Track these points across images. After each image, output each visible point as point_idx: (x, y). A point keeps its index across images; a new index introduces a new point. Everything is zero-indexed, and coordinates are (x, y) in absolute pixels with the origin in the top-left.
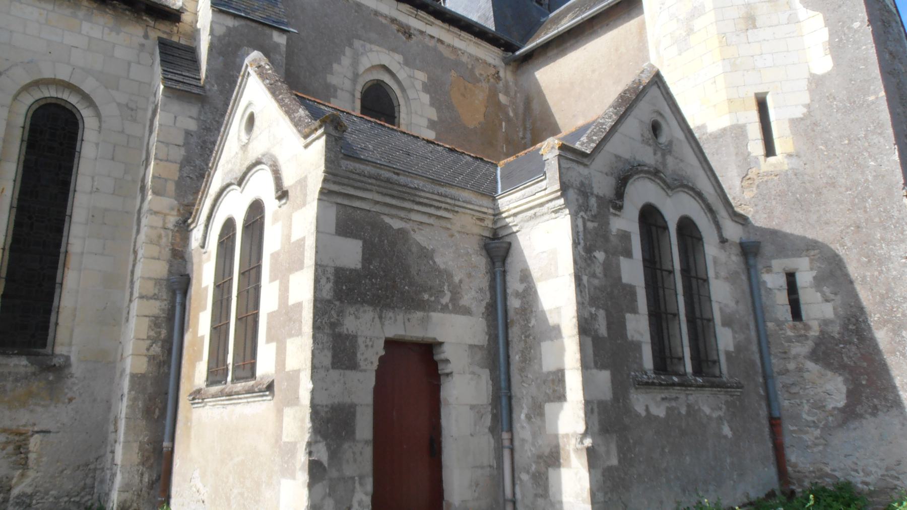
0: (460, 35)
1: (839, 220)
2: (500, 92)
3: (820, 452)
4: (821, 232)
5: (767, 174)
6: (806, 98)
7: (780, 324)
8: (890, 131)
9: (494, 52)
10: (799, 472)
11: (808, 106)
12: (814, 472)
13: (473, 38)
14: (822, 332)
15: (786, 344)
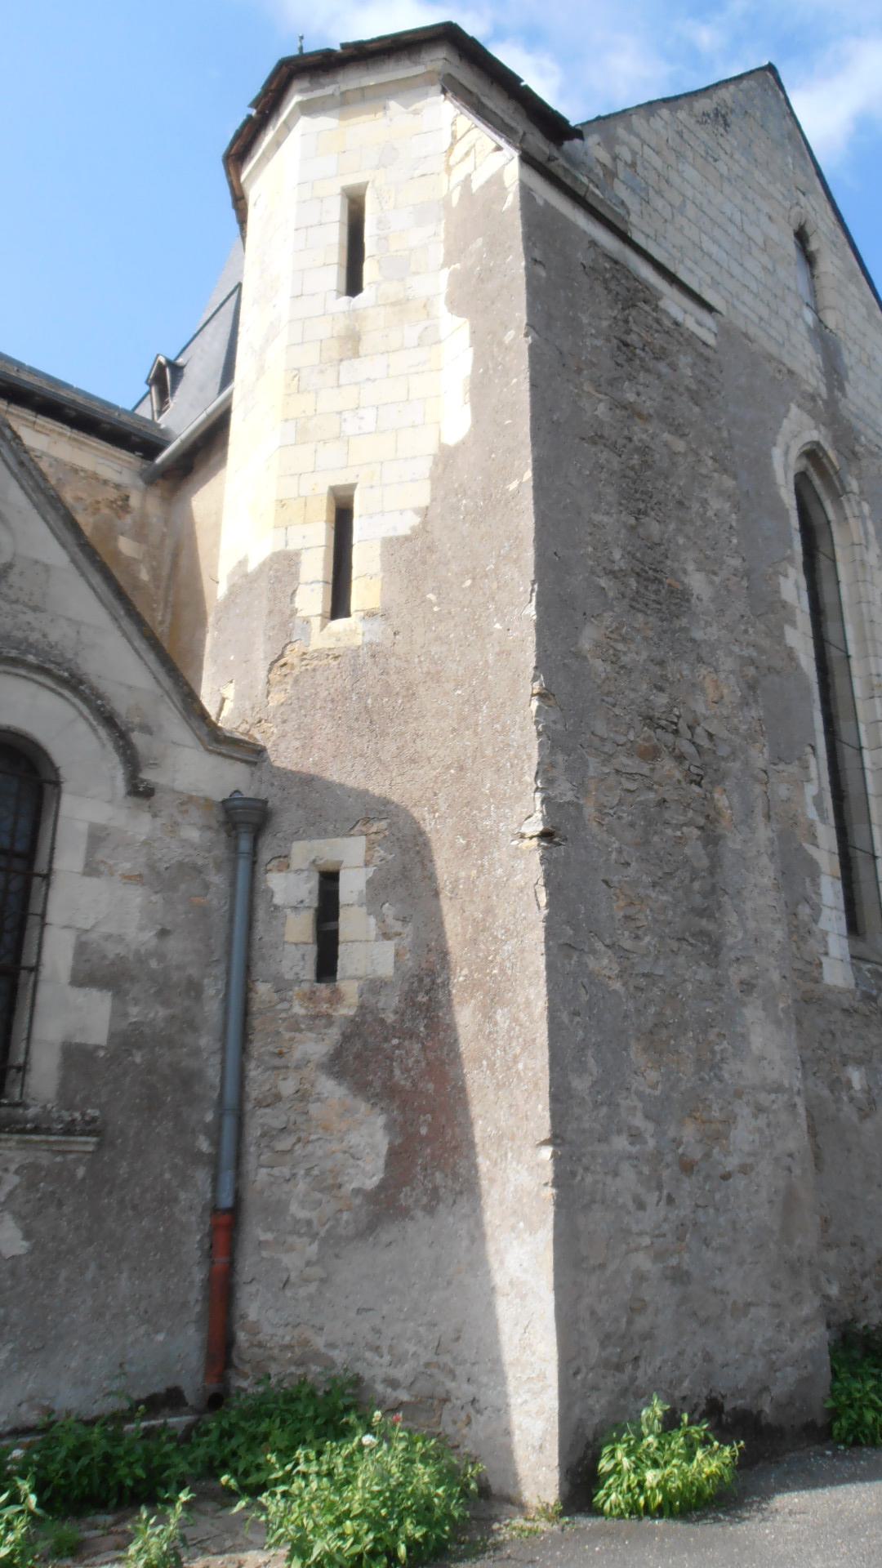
0: (34, 423)
1: (434, 755)
2: (122, 534)
3: (310, 1298)
4: (399, 780)
5: (321, 654)
6: (422, 495)
7: (282, 987)
8: (529, 554)
9: (119, 459)
10: (260, 1345)
11: (425, 513)
12: (290, 1347)
13: (67, 430)
14: (362, 1007)
15: (287, 1035)
